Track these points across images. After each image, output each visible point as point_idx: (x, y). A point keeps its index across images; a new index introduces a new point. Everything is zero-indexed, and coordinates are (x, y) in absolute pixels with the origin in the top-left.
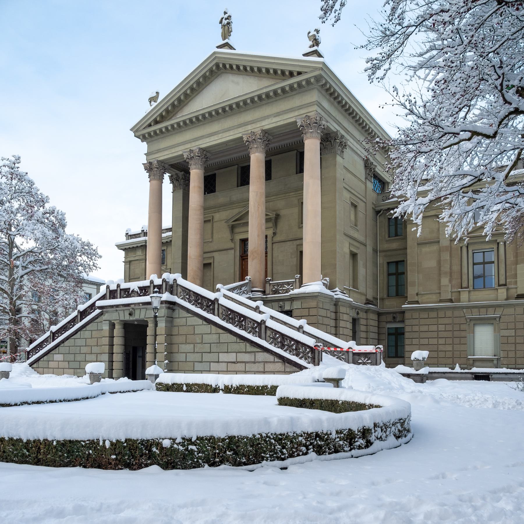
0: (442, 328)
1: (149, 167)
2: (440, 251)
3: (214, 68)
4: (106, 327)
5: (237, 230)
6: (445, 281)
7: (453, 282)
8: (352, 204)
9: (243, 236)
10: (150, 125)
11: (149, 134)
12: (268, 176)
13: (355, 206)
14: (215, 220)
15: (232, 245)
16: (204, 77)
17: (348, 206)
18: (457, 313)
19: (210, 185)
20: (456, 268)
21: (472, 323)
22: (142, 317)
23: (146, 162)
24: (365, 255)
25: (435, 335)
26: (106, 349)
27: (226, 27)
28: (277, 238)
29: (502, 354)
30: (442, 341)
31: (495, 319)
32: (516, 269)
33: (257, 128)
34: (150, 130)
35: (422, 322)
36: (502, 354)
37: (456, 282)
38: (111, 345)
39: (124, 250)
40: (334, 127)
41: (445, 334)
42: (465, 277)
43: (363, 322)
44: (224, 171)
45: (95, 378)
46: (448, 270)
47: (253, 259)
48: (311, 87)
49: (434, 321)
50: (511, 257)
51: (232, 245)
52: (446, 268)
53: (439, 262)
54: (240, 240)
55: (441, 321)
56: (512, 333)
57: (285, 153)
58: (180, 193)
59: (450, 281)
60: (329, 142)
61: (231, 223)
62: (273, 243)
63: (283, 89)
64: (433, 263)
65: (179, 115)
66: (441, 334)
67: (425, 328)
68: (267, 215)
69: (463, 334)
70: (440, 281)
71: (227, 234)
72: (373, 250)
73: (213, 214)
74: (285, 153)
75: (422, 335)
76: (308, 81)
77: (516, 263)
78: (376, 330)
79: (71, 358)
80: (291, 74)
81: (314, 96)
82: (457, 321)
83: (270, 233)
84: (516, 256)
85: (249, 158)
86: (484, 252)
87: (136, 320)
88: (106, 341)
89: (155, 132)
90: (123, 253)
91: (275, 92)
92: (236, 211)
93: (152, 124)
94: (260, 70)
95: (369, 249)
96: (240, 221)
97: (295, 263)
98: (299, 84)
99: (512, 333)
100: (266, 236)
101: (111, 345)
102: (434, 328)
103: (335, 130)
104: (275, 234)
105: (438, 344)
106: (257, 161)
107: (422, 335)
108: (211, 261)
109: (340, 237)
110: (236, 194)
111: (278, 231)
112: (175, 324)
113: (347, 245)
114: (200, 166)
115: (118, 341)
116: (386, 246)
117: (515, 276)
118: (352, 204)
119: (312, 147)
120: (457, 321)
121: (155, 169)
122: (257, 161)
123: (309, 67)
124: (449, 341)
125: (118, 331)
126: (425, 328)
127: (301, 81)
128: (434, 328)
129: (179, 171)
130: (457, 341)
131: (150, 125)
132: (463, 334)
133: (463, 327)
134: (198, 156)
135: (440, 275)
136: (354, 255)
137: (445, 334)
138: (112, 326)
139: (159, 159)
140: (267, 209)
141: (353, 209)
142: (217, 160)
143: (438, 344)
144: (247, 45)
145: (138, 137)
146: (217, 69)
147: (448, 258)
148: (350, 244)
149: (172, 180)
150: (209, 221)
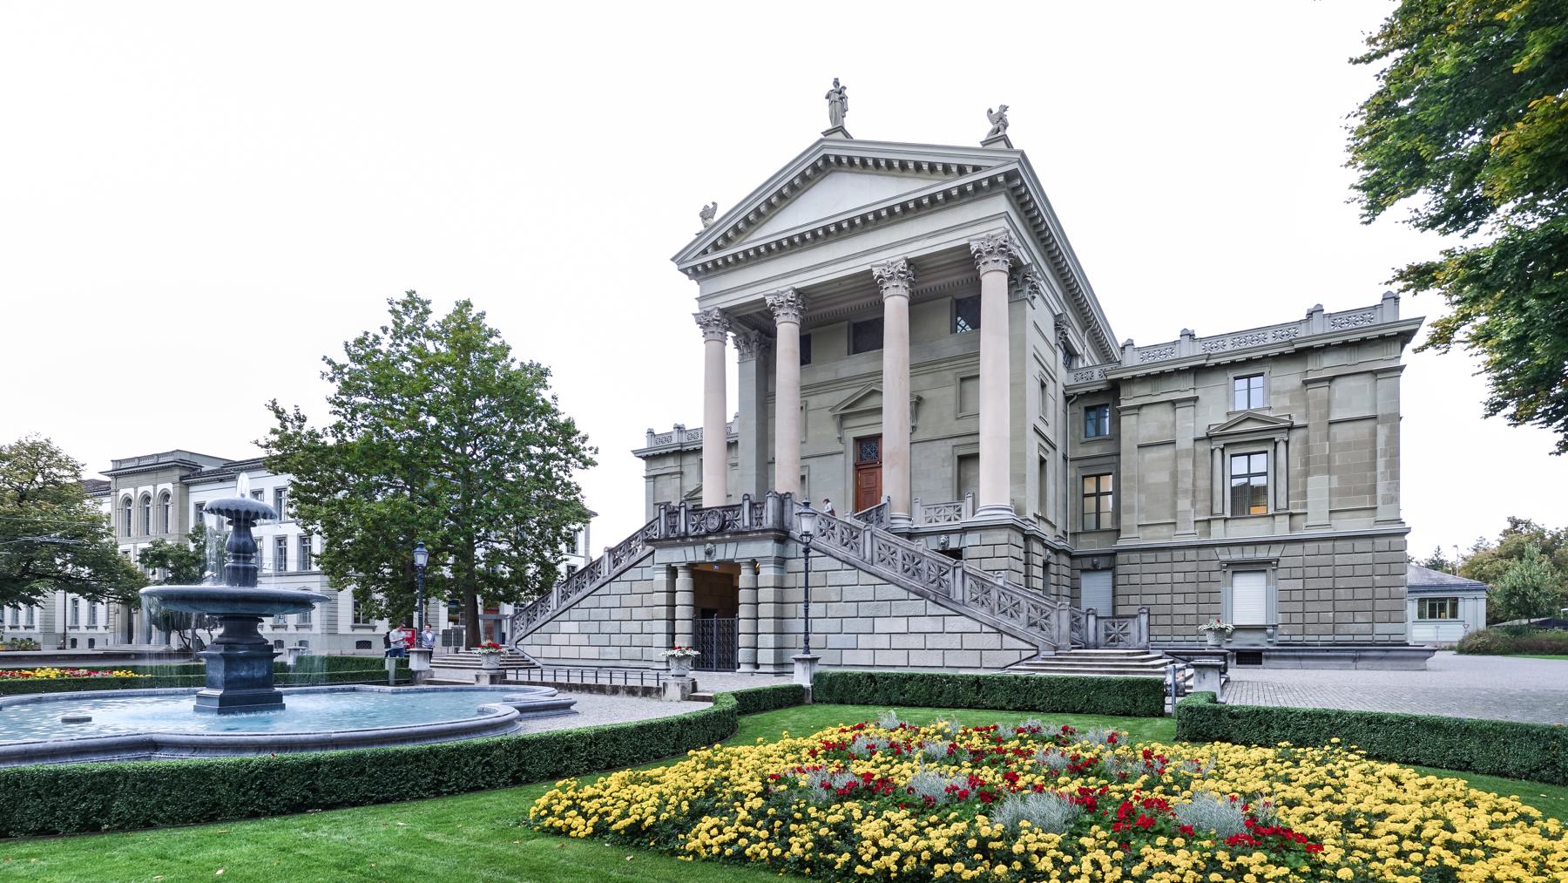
0: (1179, 577)
1: (704, 321)
2: (1176, 457)
3: (820, 163)
4: (661, 578)
6: (1184, 504)
7: (1198, 506)
10: (705, 252)
11: (704, 265)
12: (805, 359)
15: (841, 448)
16: (803, 176)
18: (1204, 554)
20: (1203, 484)
21: (1230, 572)
22: (730, 556)
25: (1167, 588)
26: (662, 612)
27: (838, 98)
29: (1281, 618)
30: (1179, 599)
31: (1269, 562)
32: (1305, 485)
33: (787, 286)
34: (704, 262)
35: (1146, 568)
36: (1281, 618)
37: (1203, 505)
38: (672, 606)
40: (1025, 259)
41: (1186, 588)
42: (1218, 498)
44: (842, 322)
46: (1189, 486)
47: (892, 467)
48: (881, 223)
49: (1167, 567)
50: (1297, 466)
52: (1186, 483)
53: (1174, 476)
55: (1177, 567)
56: (1299, 584)
57: (947, 293)
59: (1193, 504)
60: (1018, 276)
61: (838, 411)
63: (947, 194)
64: (1164, 477)
65: (756, 236)
66: (1177, 588)
67: (1151, 579)
69: (1214, 587)
70: (1175, 505)
71: (831, 430)
74: (947, 293)
75: (1146, 589)
76: (993, 181)
77: (1306, 474)
79: (594, 627)
80: (962, 170)
81: (1000, 204)
82: (1205, 566)
84: (1307, 462)
85: (880, 306)
86: (1249, 455)
87: (718, 563)
88: (662, 598)
89: (714, 262)
90: (643, 462)
91: (932, 198)
92: (848, 393)
94: (903, 166)
96: (864, 403)
97: (950, 475)
98: (977, 186)
99: (1299, 584)
101: (672, 606)
102: (1166, 578)
105: (1172, 604)
106: (895, 307)
107: (1146, 589)
109: (1030, 433)
110: (860, 364)
115: (683, 598)
116: (1082, 452)
117: (1304, 494)
119: (994, 284)
120: (1205, 566)
122: (895, 307)
123: (995, 159)
124: (1191, 598)
125: (683, 580)
126: (1151, 579)
127: (980, 181)
128: (1166, 578)
129: (752, 327)
130: (1204, 598)
131: (705, 252)
132: (1214, 587)
133: (1214, 576)
135: (1175, 494)
136: (1043, 462)
137: (1186, 588)
138: (672, 571)
142: (844, 306)
143: (1172, 604)
144: (865, 126)
145: (684, 271)
146: (822, 166)
147: (1190, 467)
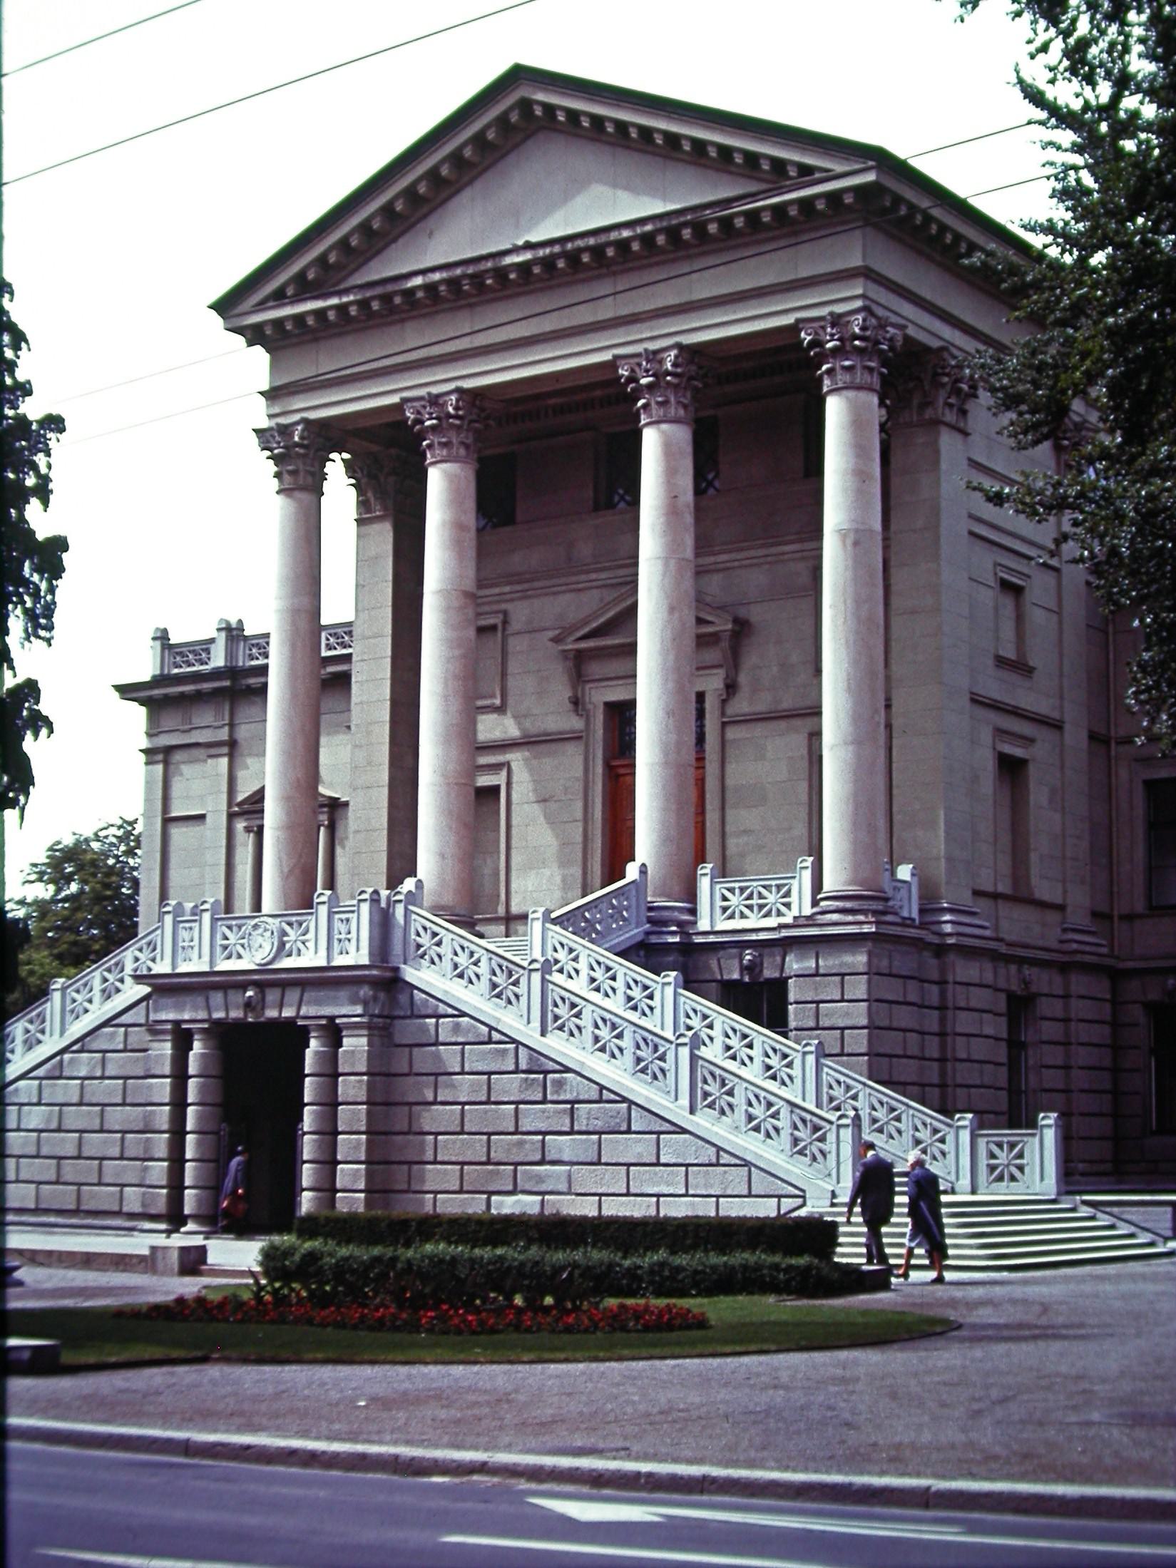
5: (595, 669)
8: (1005, 585)
9: (616, 694)
13: (1014, 591)
14: (515, 626)
15: (576, 723)
17: (987, 597)
19: (494, 506)
23: (265, 423)
24: (1056, 767)
28: (741, 705)
39: (142, 702)
43: (1048, 1007)
45: (331, 1255)
51: (576, 723)
54: (607, 704)
58: (384, 535)
62: (724, 724)
68: (700, 621)
71: (561, 690)
72: (1093, 737)
73: (503, 606)
78: (1101, 1033)
83: (713, 684)
90: (137, 714)
93: (290, 291)
95: (1076, 736)
100: (700, 697)
103: (935, 344)
104: (731, 688)
108: (499, 779)
111: (743, 679)
112: (398, 1039)
113: (986, 736)
114: (462, 452)
118: (1005, 585)
121: (297, 457)
129: (388, 462)
134: (456, 417)
139: (313, 415)
140: (700, 599)
141: (1008, 602)
148: (1000, 732)
149: (350, 468)
150: (493, 628)
